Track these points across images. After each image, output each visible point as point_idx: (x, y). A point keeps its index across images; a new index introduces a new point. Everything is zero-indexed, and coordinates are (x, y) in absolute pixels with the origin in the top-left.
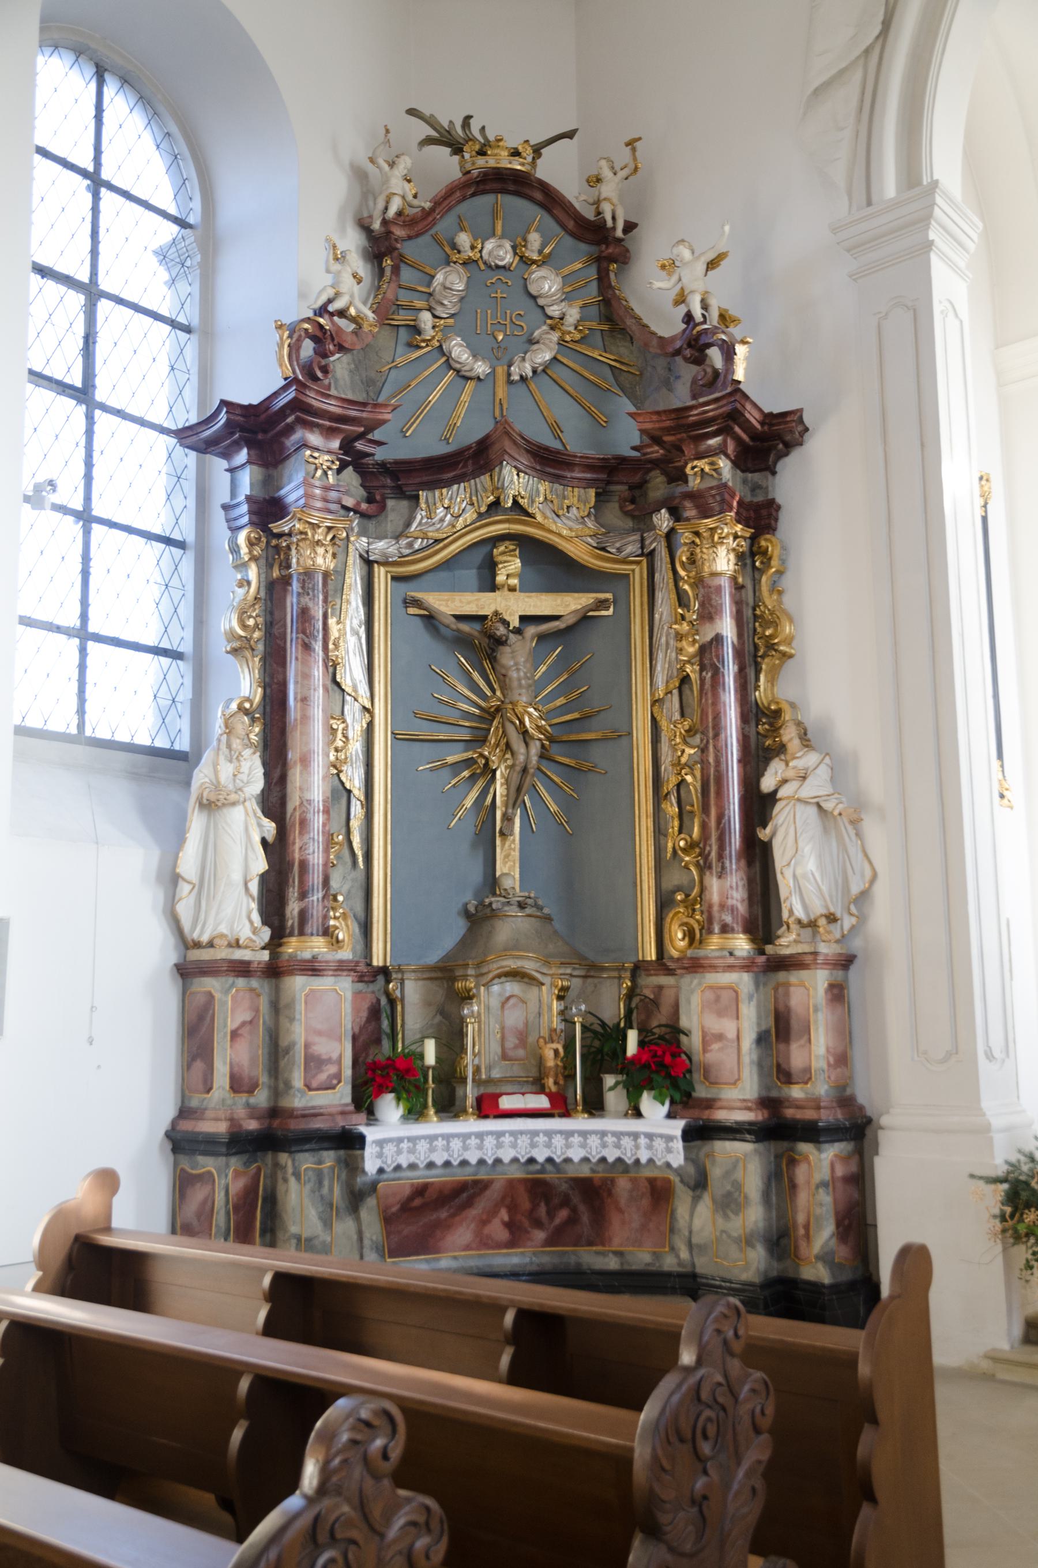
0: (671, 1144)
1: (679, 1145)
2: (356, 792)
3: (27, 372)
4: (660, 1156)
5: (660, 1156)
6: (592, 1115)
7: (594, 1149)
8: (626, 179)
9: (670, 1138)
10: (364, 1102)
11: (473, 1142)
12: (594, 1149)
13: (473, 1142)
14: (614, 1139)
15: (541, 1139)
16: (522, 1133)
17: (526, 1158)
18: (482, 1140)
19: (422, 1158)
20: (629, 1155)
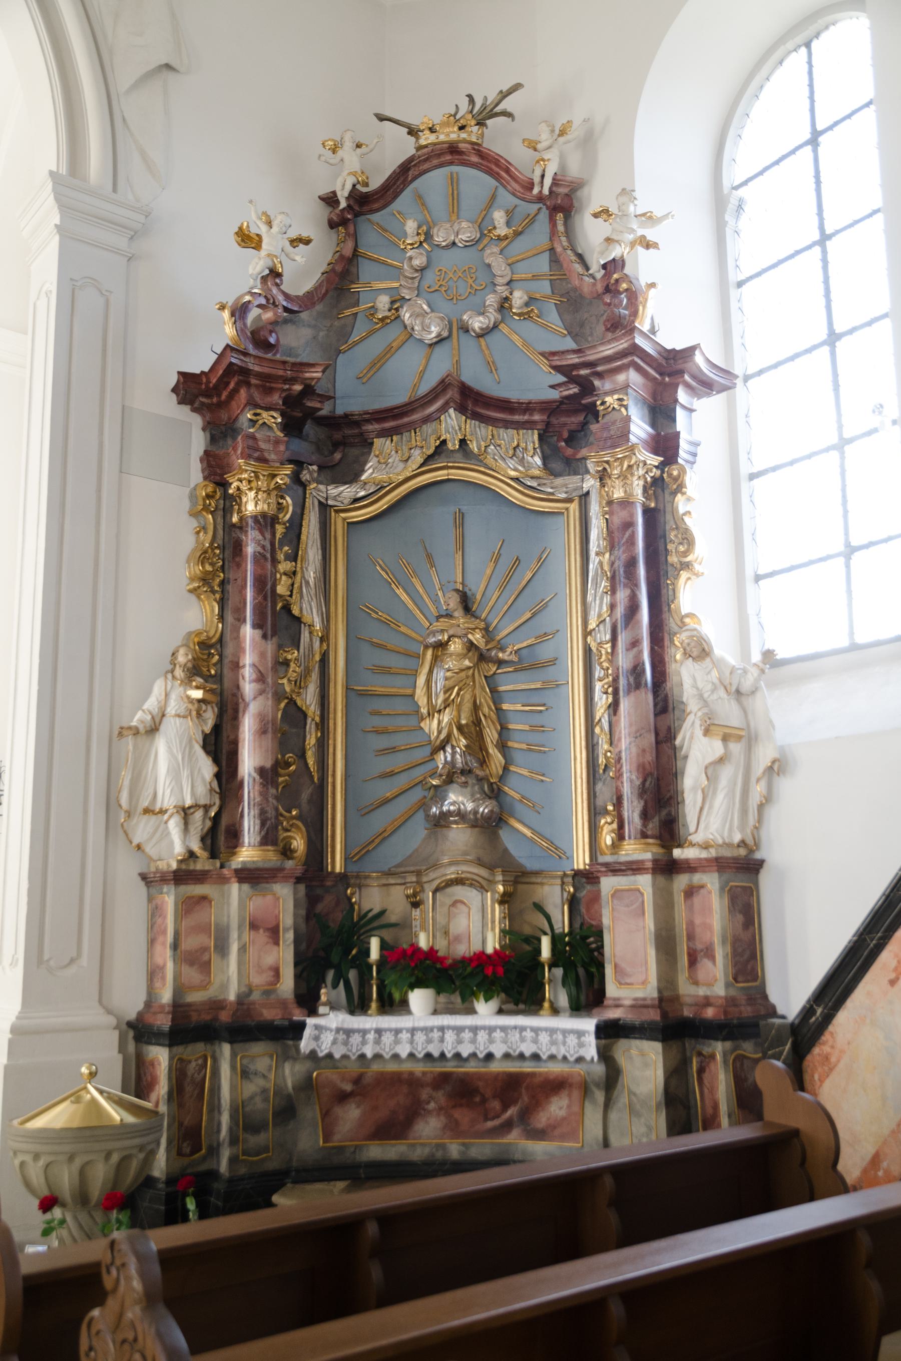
0: (583, 1039)
1: (591, 1040)
2: (310, 713)
3: (660, 247)
4: (544, 1050)
5: (572, 1052)
6: (352, 1012)
7: (544, 1045)
8: (381, 118)
9: (580, 1034)
10: (308, 1001)
11: (467, 1035)
12: (544, 1045)
13: (467, 1035)
14: (533, 1034)
15: (529, 1034)
16: (449, 1027)
17: (390, 1054)
18: (476, 1034)
19: (354, 1050)
20: (387, 1050)
